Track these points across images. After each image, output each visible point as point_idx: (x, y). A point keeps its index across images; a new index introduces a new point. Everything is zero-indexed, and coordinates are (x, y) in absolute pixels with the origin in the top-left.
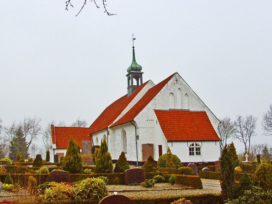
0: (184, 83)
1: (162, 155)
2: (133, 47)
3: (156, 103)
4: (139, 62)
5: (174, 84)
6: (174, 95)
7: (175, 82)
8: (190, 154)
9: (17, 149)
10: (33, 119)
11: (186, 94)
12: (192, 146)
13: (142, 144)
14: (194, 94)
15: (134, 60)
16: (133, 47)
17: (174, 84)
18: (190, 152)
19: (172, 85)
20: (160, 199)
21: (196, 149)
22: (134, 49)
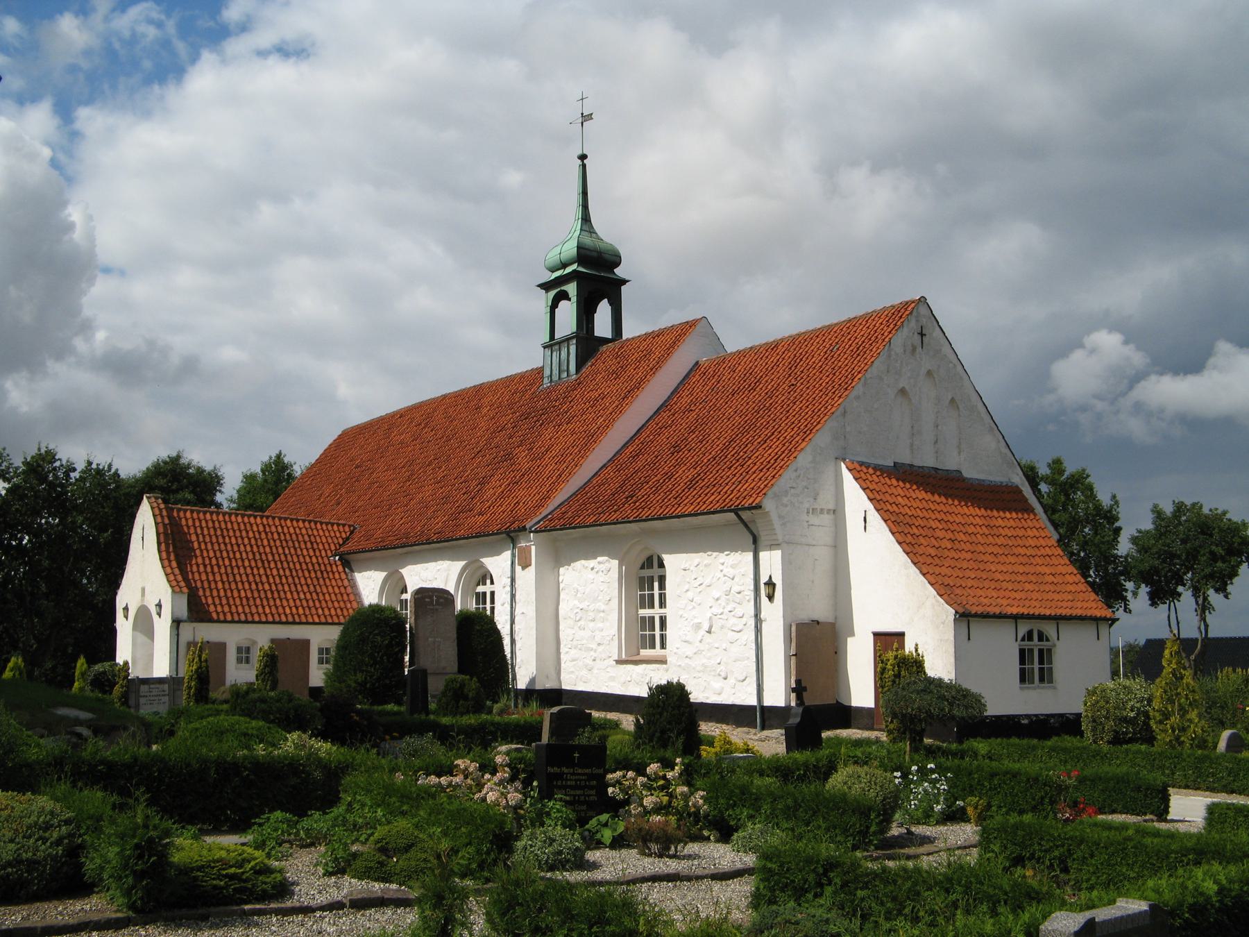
0: (946, 349)
1: (224, 684)
2: (583, 157)
3: (848, 429)
4: (608, 231)
5: (914, 349)
6: (910, 400)
7: (917, 338)
8: (1024, 677)
9: (1111, 892)
10: (223, 490)
11: (953, 400)
12: (1026, 642)
13: (225, 644)
14: (980, 405)
15: (586, 219)
16: (583, 157)
17: (914, 349)
18: (1020, 669)
19: (905, 351)
20: (179, 926)
21: (1041, 652)
22: (584, 166)
